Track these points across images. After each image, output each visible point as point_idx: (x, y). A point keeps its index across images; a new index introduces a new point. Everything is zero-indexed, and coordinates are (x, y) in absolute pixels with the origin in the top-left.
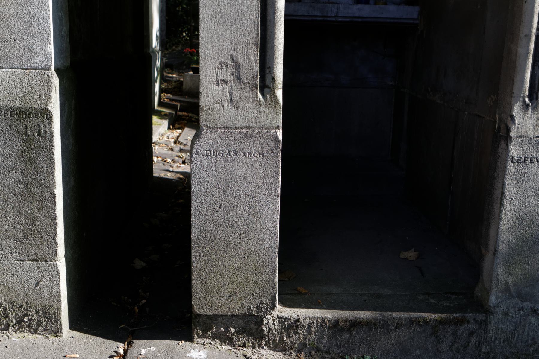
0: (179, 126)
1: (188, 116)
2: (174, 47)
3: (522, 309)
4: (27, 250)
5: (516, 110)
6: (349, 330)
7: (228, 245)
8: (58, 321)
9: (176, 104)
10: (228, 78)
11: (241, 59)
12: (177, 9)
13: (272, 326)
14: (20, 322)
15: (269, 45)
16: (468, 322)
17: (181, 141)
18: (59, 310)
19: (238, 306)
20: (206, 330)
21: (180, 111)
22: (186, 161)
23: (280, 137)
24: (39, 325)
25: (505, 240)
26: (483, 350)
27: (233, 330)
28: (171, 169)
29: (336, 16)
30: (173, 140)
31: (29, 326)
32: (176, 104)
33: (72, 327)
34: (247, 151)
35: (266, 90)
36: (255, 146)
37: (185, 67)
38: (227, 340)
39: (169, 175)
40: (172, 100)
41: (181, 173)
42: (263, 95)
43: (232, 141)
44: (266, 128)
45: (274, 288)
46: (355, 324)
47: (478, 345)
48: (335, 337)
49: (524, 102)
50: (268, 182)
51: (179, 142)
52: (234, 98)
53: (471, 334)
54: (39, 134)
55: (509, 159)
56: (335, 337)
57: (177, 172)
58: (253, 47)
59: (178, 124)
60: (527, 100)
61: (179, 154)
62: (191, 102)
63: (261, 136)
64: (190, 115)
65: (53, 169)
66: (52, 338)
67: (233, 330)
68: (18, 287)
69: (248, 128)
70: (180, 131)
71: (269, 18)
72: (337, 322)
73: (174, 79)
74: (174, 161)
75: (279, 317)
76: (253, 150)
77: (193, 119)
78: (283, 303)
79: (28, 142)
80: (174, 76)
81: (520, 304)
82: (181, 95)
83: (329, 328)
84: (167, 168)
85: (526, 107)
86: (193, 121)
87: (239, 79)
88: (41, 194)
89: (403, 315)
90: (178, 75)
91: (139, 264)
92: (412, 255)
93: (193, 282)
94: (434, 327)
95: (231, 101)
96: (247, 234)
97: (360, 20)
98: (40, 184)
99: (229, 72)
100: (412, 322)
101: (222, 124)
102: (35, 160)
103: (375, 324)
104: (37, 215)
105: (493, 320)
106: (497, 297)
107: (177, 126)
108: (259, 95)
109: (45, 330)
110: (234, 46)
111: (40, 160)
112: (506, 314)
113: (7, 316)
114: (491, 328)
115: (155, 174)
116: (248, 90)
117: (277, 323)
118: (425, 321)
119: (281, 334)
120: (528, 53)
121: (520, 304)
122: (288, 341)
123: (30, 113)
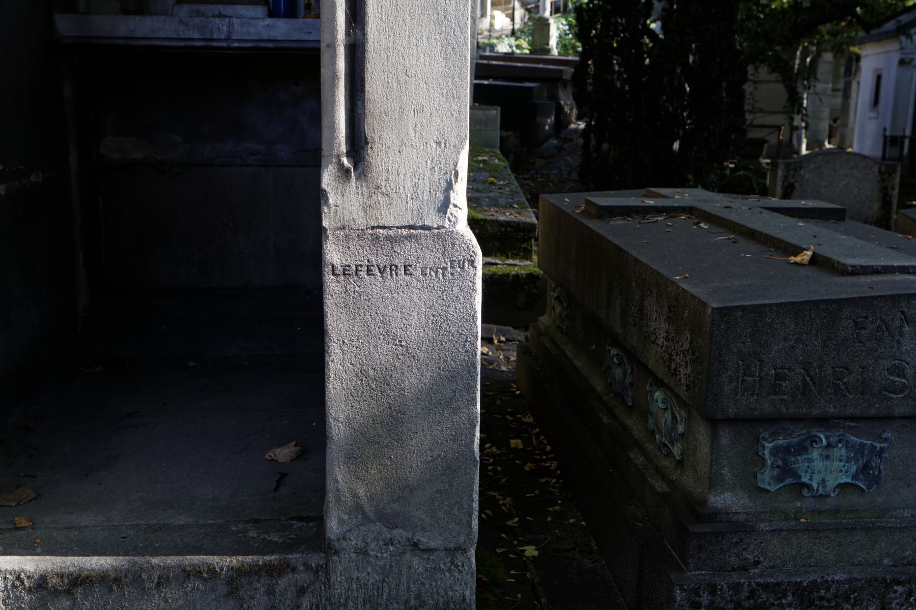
3: (391, 542)
5: (328, 179)
16: (294, 570)
25: (342, 417)
29: (228, 39)
49: (341, 165)
53: (301, 591)
55: (327, 270)
60: (345, 161)
83: (29, 591)
94: (230, 581)
97: (271, 45)
100: (188, 574)
103: (117, 580)
106: (341, 522)
112: (363, 552)
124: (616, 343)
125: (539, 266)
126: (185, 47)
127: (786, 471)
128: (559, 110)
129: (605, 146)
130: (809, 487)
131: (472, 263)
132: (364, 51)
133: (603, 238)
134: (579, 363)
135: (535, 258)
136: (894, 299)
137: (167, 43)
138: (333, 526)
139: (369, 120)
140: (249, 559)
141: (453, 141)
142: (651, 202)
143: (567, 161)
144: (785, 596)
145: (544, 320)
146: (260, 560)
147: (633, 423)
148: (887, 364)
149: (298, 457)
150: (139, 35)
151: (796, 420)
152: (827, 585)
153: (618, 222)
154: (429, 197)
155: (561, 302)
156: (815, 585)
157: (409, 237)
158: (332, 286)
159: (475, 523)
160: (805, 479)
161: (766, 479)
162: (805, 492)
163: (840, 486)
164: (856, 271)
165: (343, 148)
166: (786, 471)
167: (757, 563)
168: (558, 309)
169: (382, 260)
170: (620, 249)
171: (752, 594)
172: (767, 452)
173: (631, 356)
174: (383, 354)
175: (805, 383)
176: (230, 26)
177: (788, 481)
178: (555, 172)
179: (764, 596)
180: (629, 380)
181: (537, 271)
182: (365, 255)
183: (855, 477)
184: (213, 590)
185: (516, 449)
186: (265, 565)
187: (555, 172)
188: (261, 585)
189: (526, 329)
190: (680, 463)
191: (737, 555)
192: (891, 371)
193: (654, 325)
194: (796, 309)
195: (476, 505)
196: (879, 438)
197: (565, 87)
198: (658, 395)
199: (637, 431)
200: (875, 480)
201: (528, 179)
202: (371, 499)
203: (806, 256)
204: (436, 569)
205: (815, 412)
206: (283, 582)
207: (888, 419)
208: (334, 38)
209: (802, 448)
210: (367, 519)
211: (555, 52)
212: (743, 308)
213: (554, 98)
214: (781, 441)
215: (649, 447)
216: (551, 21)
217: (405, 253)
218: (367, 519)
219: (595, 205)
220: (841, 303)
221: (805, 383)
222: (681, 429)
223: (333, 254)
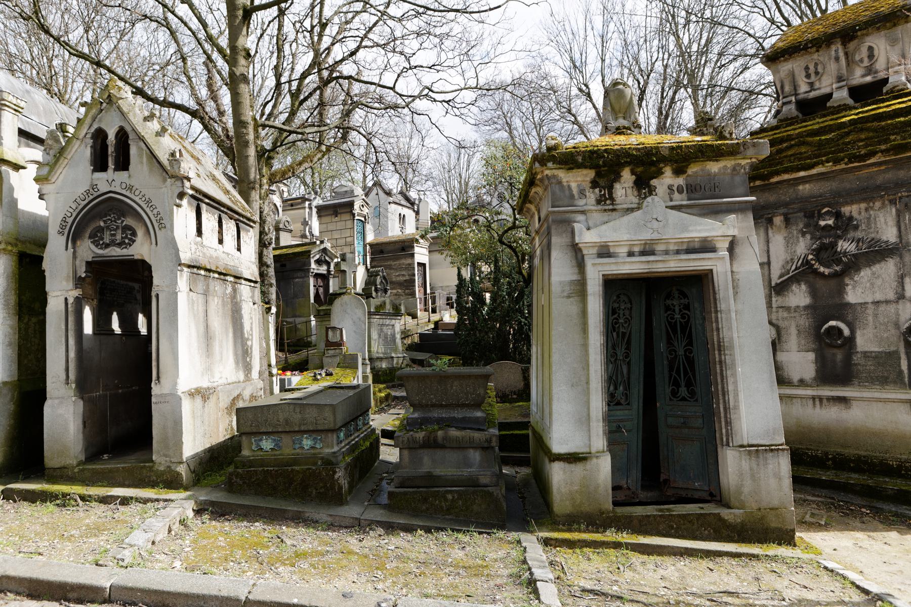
5: (153, 385)
166: (258, 445)
209: (261, 440)
223: (153, 400)
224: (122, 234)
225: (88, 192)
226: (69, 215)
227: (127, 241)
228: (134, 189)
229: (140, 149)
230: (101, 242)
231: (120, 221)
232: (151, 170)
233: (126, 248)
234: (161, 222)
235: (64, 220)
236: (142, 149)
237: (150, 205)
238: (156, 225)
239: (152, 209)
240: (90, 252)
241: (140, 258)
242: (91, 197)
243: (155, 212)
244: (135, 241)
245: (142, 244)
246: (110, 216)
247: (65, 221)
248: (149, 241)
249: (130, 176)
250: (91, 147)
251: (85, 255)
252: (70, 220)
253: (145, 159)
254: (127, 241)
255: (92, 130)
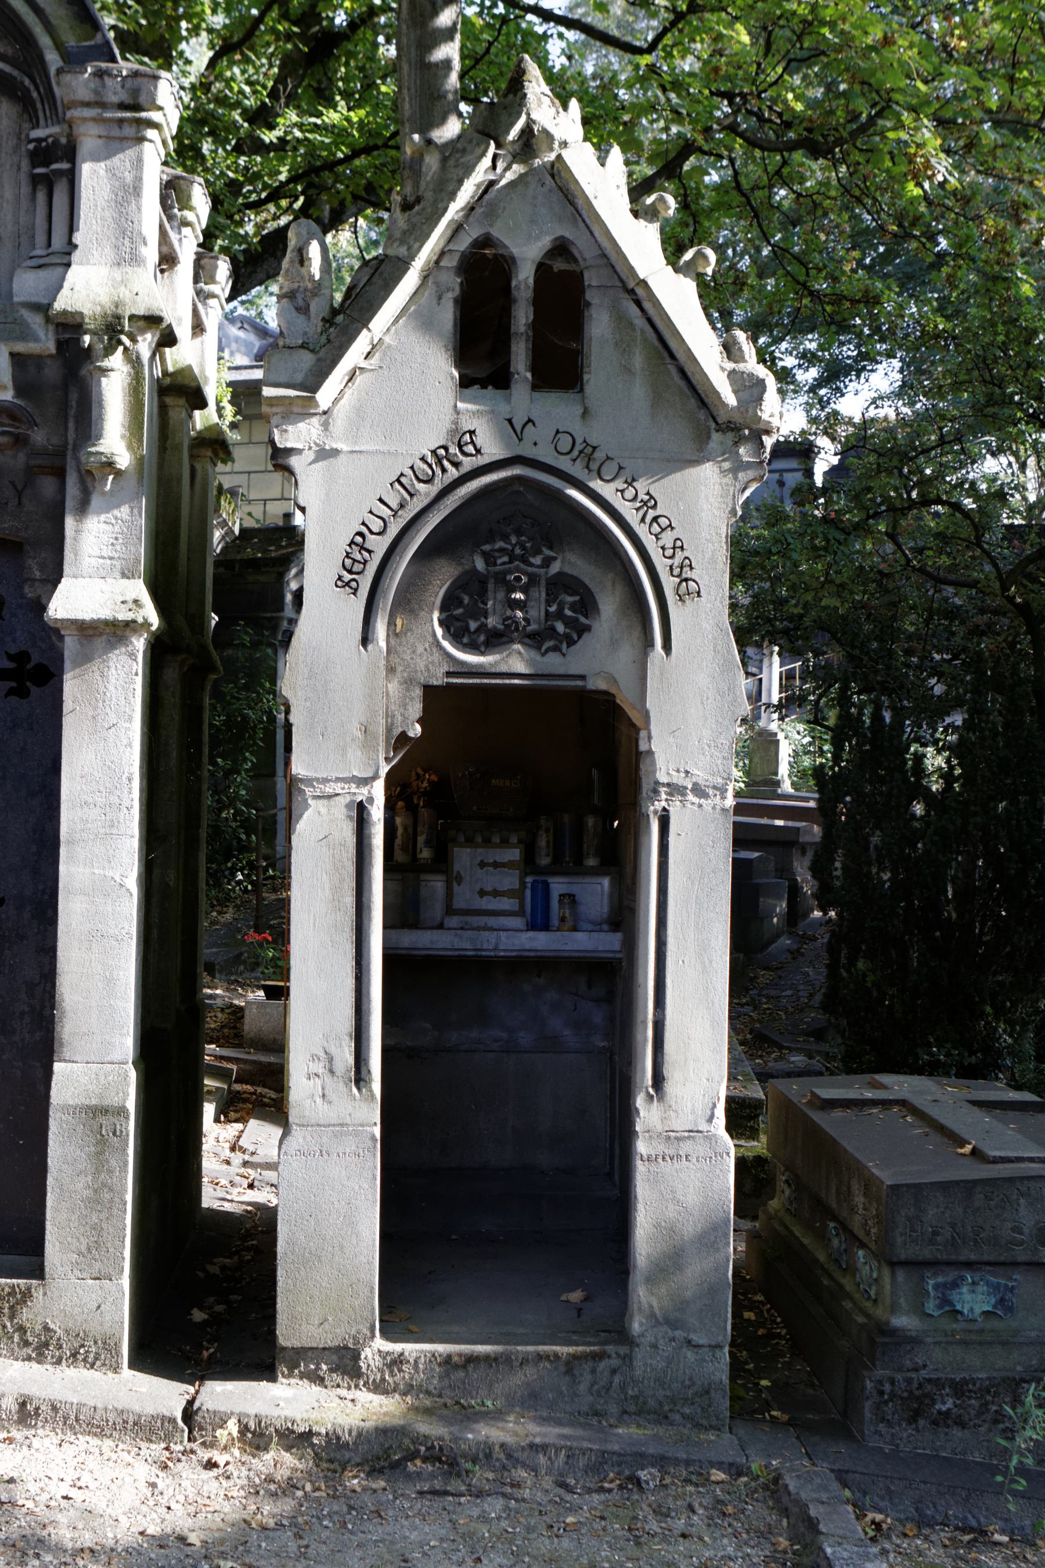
0: (238, 1115)
1: (254, 1093)
2: (214, 914)
3: (673, 1339)
4: (90, 1266)
5: (640, 1101)
6: (465, 1367)
7: (320, 1261)
8: (119, 1354)
9: (230, 1066)
10: (320, 1071)
11: (333, 1050)
12: (224, 815)
13: (371, 1362)
14: (74, 1355)
15: (364, 1036)
16: (609, 1357)
17: (245, 1146)
18: (120, 1340)
19: (330, 1336)
20: (293, 1366)
21: (236, 1081)
22: (256, 1183)
23: (378, 1135)
24: (96, 1359)
25: (644, 1253)
26: (630, 1392)
27: (324, 1367)
28: (229, 1197)
29: (496, 949)
30: (228, 1145)
31: (85, 1360)
32: (230, 1066)
33: (130, 1367)
34: (341, 1150)
35: (362, 1083)
36: (350, 1145)
37: (242, 968)
38: (318, 1379)
39: (228, 1207)
40: (222, 1058)
41: (249, 1204)
42: (359, 1089)
43: (325, 1139)
44: (362, 1125)
45: (373, 1313)
46: (471, 1360)
47: (623, 1387)
48: (448, 1375)
49: (648, 1093)
50: (366, 1186)
51: (241, 1148)
52: (327, 1092)
53: (614, 1372)
54: (114, 1134)
55: (638, 1157)
56: (448, 1375)
57: (242, 1203)
58: (347, 1038)
59: (236, 1111)
60: (651, 1090)
61: (242, 1170)
62: (260, 1063)
63: (356, 1134)
64: (259, 1090)
65: (126, 1172)
66: (110, 1374)
67: (324, 1367)
68: (77, 1310)
69: (342, 1125)
70: (239, 1126)
71: (364, 1007)
72: (449, 1357)
73: (219, 1002)
74: (232, 1184)
75: (379, 1351)
76: (348, 1150)
77: (266, 1100)
78: (386, 1334)
79: (102, 1142)
80: (218, 992)
81: (670, 1333)
82: (239, 1046)
83: (440, 1365)
84: (221, 1194)
85: (650, 1098)
86: (266, 1105)
87: (332, 1072)
88: (111, 1201)
89: (530, 1348)
90: (228, 990)
91: (198, 1316)
92: (576, 1296)
93: (279, 1306)
94: (567, 1363)
95: (324, 1095)
96: (342, 1247)
97: (532, 954)
98: (111, 1190)
99: (322, 1064)
100: (540, 1357)
101: (313, 1122)
102: (108, 1162)
103: (496, 1359)
104: (104, 1225)
105: (639, 1354)
106: (641, 1324)
107: (232, 1115)
108: (355, 1090)
109: (104, 1365)
110: (326, 1037)
111: (113, 1163)
112: (654, 1346)
113: (61, 1347)
114: (638, 1363)
115: (205, 1204)
116: (341, 1084)
117: (377, 1358)
118: (556, 1355)
119: (382, 1372)
120: (645, 1040)
121: (670, 1333)
122: (391, 1381)
123: (107, 1111)
124: (835, 1218)
125: (768, 1150)
126: (459, 956)
127: (945, 1301)
128: (794, 891)
129: (861, 965)
130: (961, 1313)
131: (728, 1154)
132: (663, 1025)
133: (822, 1130)
134: (806, 1241)
135: (763, 1138)
136: (1010, 1180)
137: (443, 953)
138: (636, 1326)
139: (666, 1066)
140: (580, 1348)
141: (717, 1078)
142: (869, 1095)
143: (807, 974)
144: (944, 1388)
145: (774, 1204)
146: (588, 1349)
147: (846, 1282)
148: (1010, 1225)
149: (585, 1300)
150: (420, 946)
151: (949, 1264)
152: (973, 1381)
153: (838, 1114)
154: (703, 1113)
155: (789, 1185)
156: (965, 1382)
157: (689, 1137)
158: (641, 1169)
159: (729, 1327)
160: (959, 1307)
161: (931, 1306)
162: (959, 1317)
163: (985, 1313)
164: (996, 1161)
165: (650, 1083)
166: (945, 1301)
167: (925, 1366)
168: (787, 1192)
169: (671, 1152)
170: (835, 1140)
171: (920, 1386)
172: (930, 1288)
173: (844, 1227)
174: (671, 1212)
175: (953, 1238)
176: (498, 938)
177: (947, 1308)
178: (789, 993)
179: (929, 1387)
180: (844, 1246)
181: (764, 1152)
182: (661, 1148)
183: (994, 1307)
184: (556, 1369)
185: (749, 1320)
186: (591, 1352)
187: (789, 993)
188: (587, 1366)
189: (755, 1218)
190: (875, 1301)
191: (911, 1360)
192: (1013, 1229)
193: (856, 1199)
194: (945, 1187)
195: (730, 1315)
196: (1010, 1279)
197: (804, 853)
198: (861, 1253)
199: (849, 1287)
200: (1010, 1310)
201: (747, 1004)
202: (661, 1309)
203: (968, 1148)
204: (703, 1360)
205: (962, 1258)
206: (602, 1365)
207: (1015, 1264)
208: (646, 1018)
209: (955, 1285)
210: (658, 1323)
211: (787, 787)
212: (908, 1186)
213: (785, 871)
214: (940, 1279)
215: (857, 1296)
216: (781, 736)
217: (685, 1148)
218: (658, 1323)
219: (818, 1097)
220: (975, 1182)
221: (953, 1238)
222: (875, 1275)
223: (642, 1147)
224: (548, 603)
225: (440, 457)
226: (376, 525)
227: (560, 627)
228: (599, 455)
229: (621, 320)
230: (473, 625)
231: (537, 560)
232: (657, 400)
233: (556, 649)
234: (687, 573)
235: (359, 542)
236: (631, 325)
237: (651, 514)
238: (669, 583)
239: (656, 528)
240: (436, 656)
241: (602, 685)
242: (453, 473)
243: (667, 539)
244: (588, 629)
245: (614, 643)
246: (505, 538)
247: (362, 548)
248: (637, 632)
249: (586, 413)
250: (456, 301)
251: (421, 664)
252: (379, 545)
253: (638, 361)
254: (560, 627)
255: (463, 244)
